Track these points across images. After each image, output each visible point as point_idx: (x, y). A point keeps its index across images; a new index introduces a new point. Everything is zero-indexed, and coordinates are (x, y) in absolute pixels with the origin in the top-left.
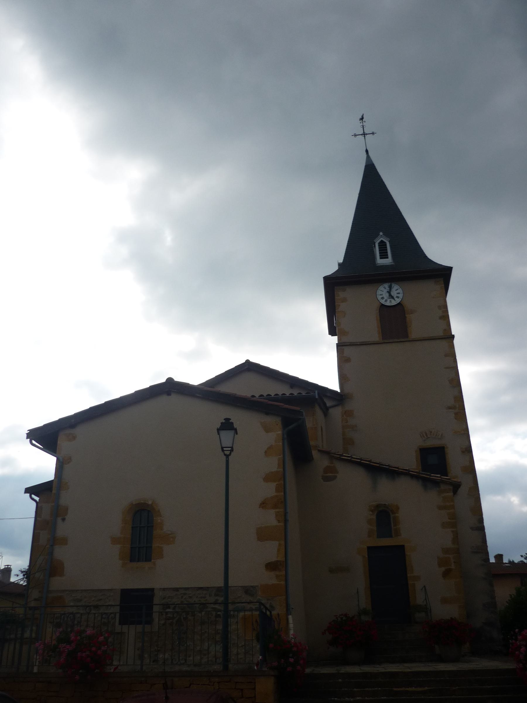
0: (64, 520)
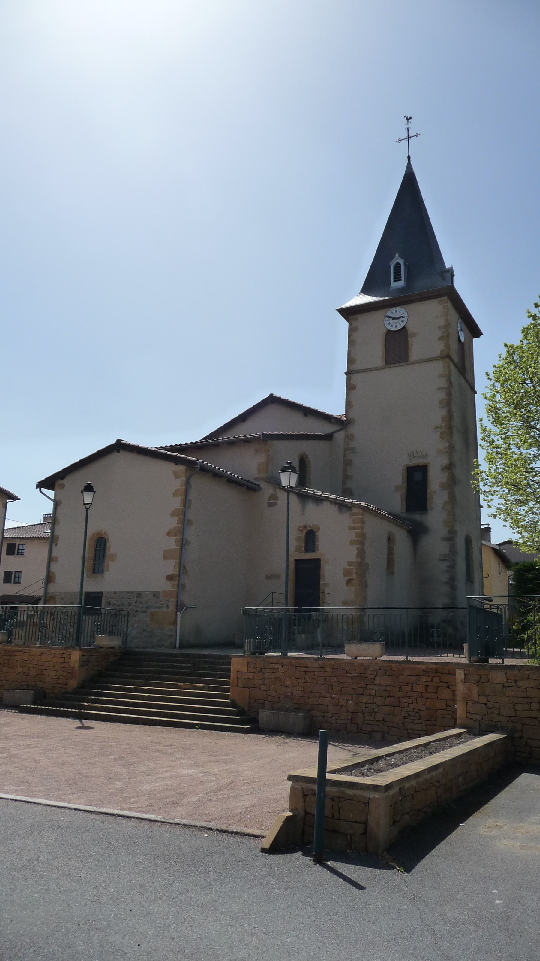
0: (56, 545)
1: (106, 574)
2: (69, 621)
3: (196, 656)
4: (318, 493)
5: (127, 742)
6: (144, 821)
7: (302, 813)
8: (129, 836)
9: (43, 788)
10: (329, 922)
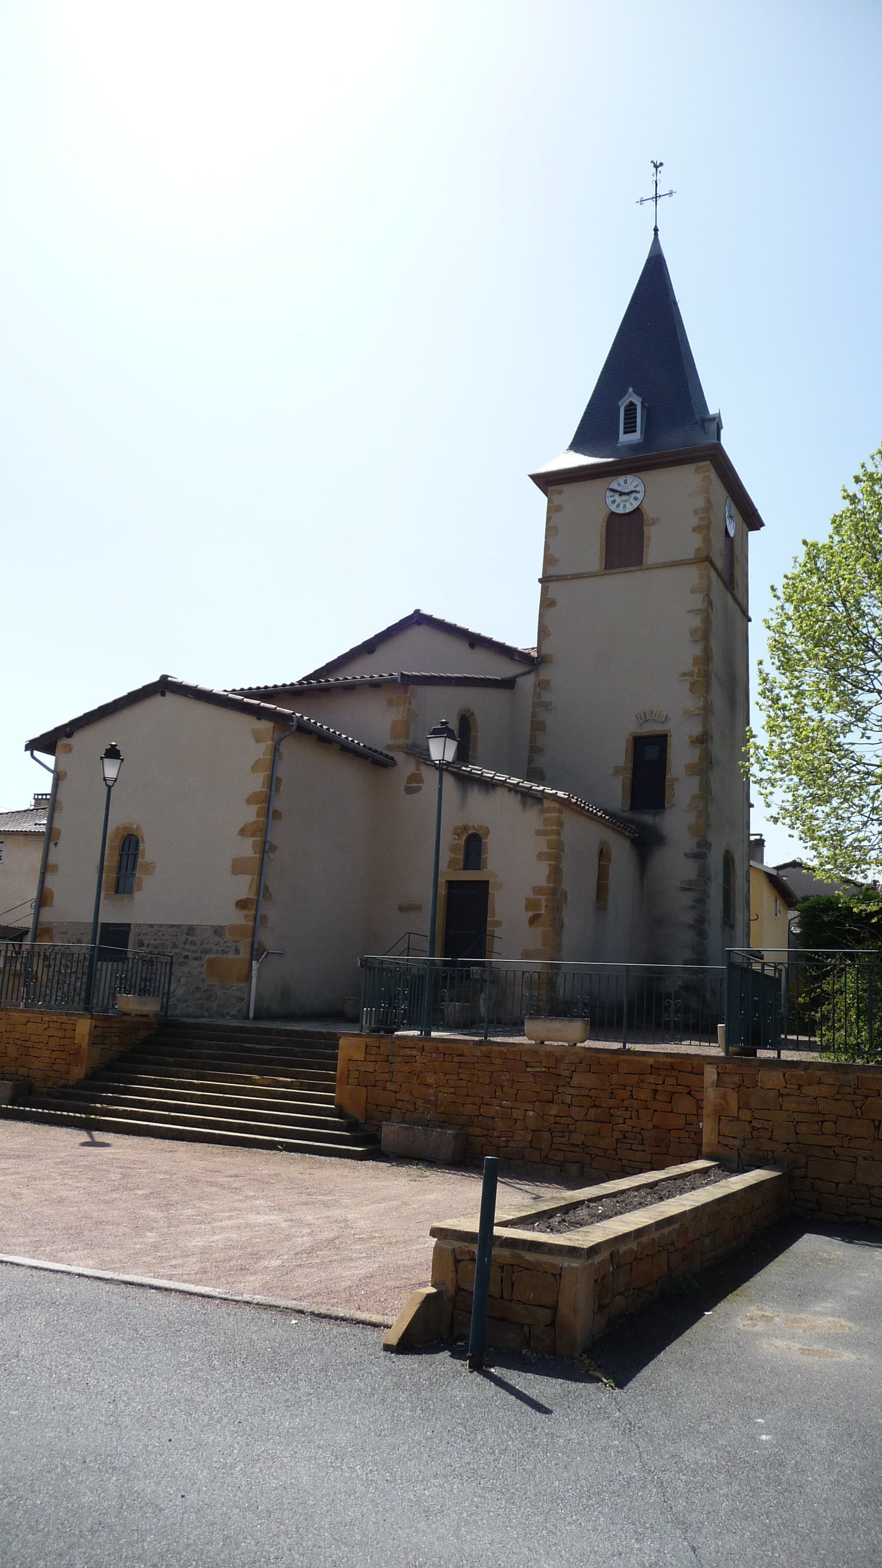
0: (56, 844)
1: (137, 895)
2: (74, 970)
3: (280, 1032)
4: (489, 774)
5: (166, 1168)
6: (192, 1297)
7: (452, 1290)
8: (168, 1320)
9: (27, 1240)
10: (492, 1465)
